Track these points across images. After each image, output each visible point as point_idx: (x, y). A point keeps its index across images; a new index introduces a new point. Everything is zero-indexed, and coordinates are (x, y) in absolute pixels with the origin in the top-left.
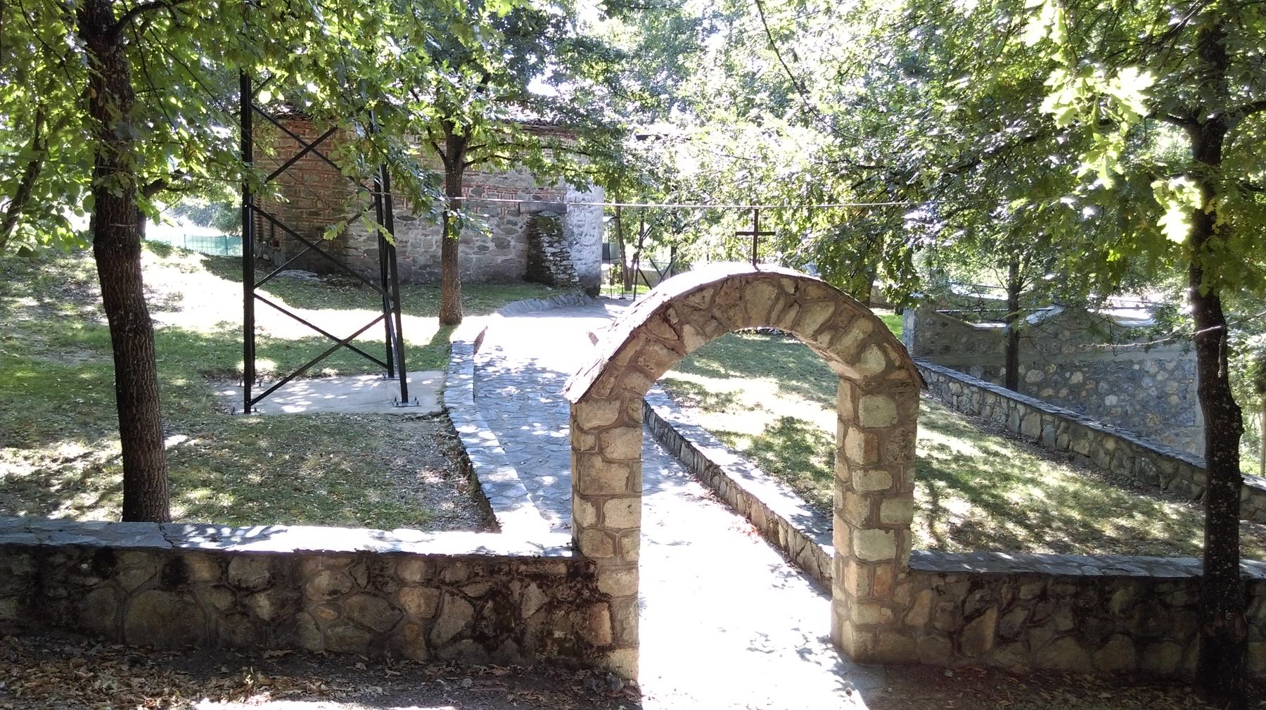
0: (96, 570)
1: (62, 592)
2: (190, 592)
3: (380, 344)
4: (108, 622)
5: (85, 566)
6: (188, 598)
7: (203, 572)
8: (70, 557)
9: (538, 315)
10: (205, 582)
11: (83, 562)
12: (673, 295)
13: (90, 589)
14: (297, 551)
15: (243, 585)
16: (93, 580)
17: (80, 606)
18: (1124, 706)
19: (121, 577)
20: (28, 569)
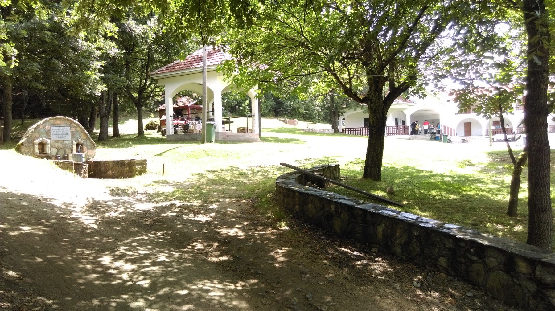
0: (476, 254)
1: (463, 260)
2: (517, 278)
3: (505, 152)
4: (480, 280)
5: (472, 250)
6: (515, 280)
7: (523, 267)
8: (467, 245)
9: (157, 143)
10: (524, 274)
11: (471, 248)
12: (385, 138)
13: (474, 262)
14: (106, 161)
15: (288, 211)
16: (475, 258)
17: (470, 269)
18: (417, 301)
19: (486, 259)
20: (451, 246)
